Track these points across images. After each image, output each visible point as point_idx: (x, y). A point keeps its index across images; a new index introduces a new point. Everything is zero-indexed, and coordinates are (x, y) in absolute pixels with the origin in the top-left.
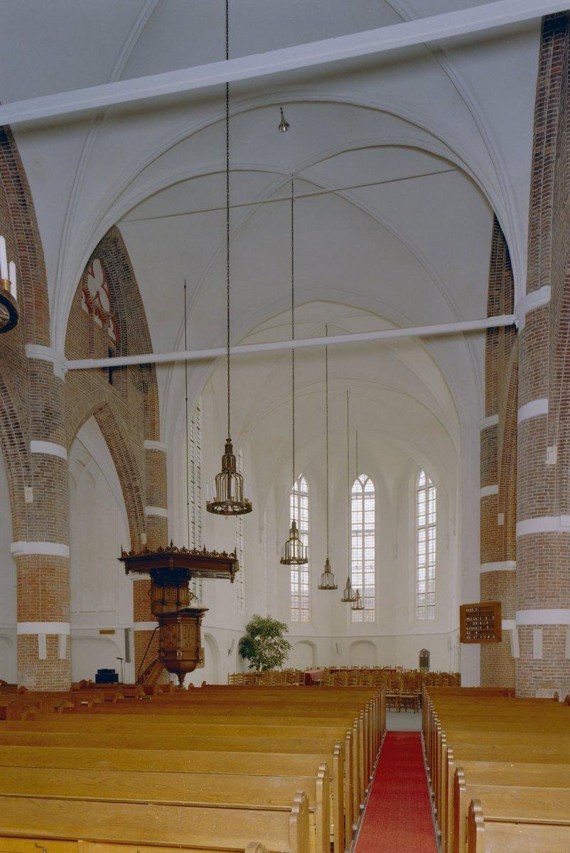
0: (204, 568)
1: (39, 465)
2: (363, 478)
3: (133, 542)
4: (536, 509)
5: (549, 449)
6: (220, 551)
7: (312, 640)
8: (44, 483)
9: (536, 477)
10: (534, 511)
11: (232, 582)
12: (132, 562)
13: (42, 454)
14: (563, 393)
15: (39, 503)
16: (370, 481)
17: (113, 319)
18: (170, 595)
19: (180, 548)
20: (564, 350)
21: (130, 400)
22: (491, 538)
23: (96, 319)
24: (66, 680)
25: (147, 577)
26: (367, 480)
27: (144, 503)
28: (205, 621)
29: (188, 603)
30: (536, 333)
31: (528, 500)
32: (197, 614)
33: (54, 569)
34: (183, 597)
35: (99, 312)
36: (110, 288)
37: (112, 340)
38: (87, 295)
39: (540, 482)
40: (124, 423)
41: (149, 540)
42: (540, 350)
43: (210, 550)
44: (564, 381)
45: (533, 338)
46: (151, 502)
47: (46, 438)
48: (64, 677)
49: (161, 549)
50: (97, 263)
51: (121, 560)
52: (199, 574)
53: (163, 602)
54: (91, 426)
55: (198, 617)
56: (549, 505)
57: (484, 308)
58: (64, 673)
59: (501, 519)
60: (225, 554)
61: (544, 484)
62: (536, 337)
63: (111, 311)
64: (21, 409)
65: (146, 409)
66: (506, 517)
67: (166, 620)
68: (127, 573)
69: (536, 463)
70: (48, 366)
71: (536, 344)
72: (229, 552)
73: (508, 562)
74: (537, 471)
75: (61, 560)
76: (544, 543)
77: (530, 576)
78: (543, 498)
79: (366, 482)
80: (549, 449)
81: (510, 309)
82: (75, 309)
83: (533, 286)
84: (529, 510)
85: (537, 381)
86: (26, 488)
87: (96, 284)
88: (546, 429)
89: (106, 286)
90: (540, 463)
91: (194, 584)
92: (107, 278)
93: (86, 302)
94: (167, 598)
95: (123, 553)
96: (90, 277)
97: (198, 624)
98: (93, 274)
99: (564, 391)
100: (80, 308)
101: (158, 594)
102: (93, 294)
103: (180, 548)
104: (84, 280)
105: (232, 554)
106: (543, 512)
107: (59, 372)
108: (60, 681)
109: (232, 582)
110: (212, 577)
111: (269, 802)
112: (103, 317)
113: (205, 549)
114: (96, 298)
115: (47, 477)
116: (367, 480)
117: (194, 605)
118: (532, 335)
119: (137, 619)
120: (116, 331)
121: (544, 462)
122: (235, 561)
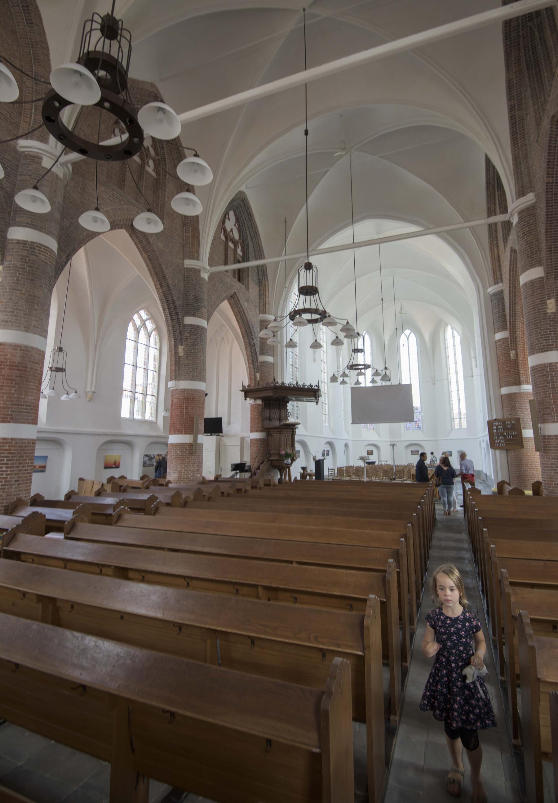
0: (298, 395)
1: (188, 331)
2: (407, 332)
3: (250, 379)
4: (543, 346)
5: (548, 301)
6: (308, 384)
7: (378, 444)
8: (191, 343)
9: (541, 322)
10: (542, 347)
11: (317, 404)
12: (248, 393)
13: (191, 325)
14: (555, 261)
15: (187, 355)
16: (412, 334)
17: (241, 244)
18: (275, 413)
19: (280, 382)
20: (551, 232)
21: (250, 290)
22: (507, 369)
23: (231, 245)
24: (199, 475)
25: (259, 402)
26: (410, 333)
27: (258, 355)
28: (299, 431)
29: (287, 419)
30: (528, 224)
31: (536, 339)
32: (292, 427)
33: (194, 398)
34: (283, 415)
35: (233, 241)
36: (239, 226)
37: (240, 255)
38: (225, 230)
39: (544, 326)
40: (246, 304)
41: (261, 378)
42: (532, 234)
43: (300, 383)
44: (554, 253)
45: (525, 227)
46: (263, 353)
47: (194, 315)
48: (198, 474)
49: (304, 385)
50: (231, 213)
51: (242, 391)
52: (294, 399)
53: (270, 419)
54: (225, 305)
55: (293, 429)
56: (554, 342)
57: (485, 215)
58: (198, 470)
59: (512, 353)
60: (311, 386)
61: (548, 327)
62: (527, 226)
63: (240, 239)
64: (179, 298)
65: (260, 296)
66: (517, 354)
67: (268, 431)
68: (246, 399)
69: (539, 312)
70: (197, 272)
71: (528, 231)
72: (314, 384)
73: (522, 386)
74: (541, 318)
75: (199, 392)
76: (554, 371)
77: (545, 397)
78: (549, 337)
79: (409, 335)
80: (548, 301)
81: (504, 210)
82: (216, 238)
83: (521, 193)
84: (538, 347)
85: (532, 255)
86: (179, 346)
87: (230, 224)
88: (544, 288)
89: (237, 225)
90: (542, 312)
91: (290, 406)
92: (237, 220)
93: (224, 235)
94: (272, 416)
95: (243, 387)
96: (227, 220)
97: (293, 434)
98: (229, 219)
99: (555, 260)
100: (220, 238)
101: (267, 413)
102: (228, 229)
103: (280, 382)
104: (223, 222)
105: (316, 386)
106: (550, 348)
107: (205, 276)
108: (194, 476)
109: (317, 404)
110: (303, 401)
111: (316, 638)
112: (233, 241)
113: (297, 383)
114: (230, 232)
115: (193, 339)
116: (410, 333)
117: (291, 420)
118: (524, 225)
119: (251, 432)
120: (243, 250)
121: (546, 311)
122: (318, 390)
